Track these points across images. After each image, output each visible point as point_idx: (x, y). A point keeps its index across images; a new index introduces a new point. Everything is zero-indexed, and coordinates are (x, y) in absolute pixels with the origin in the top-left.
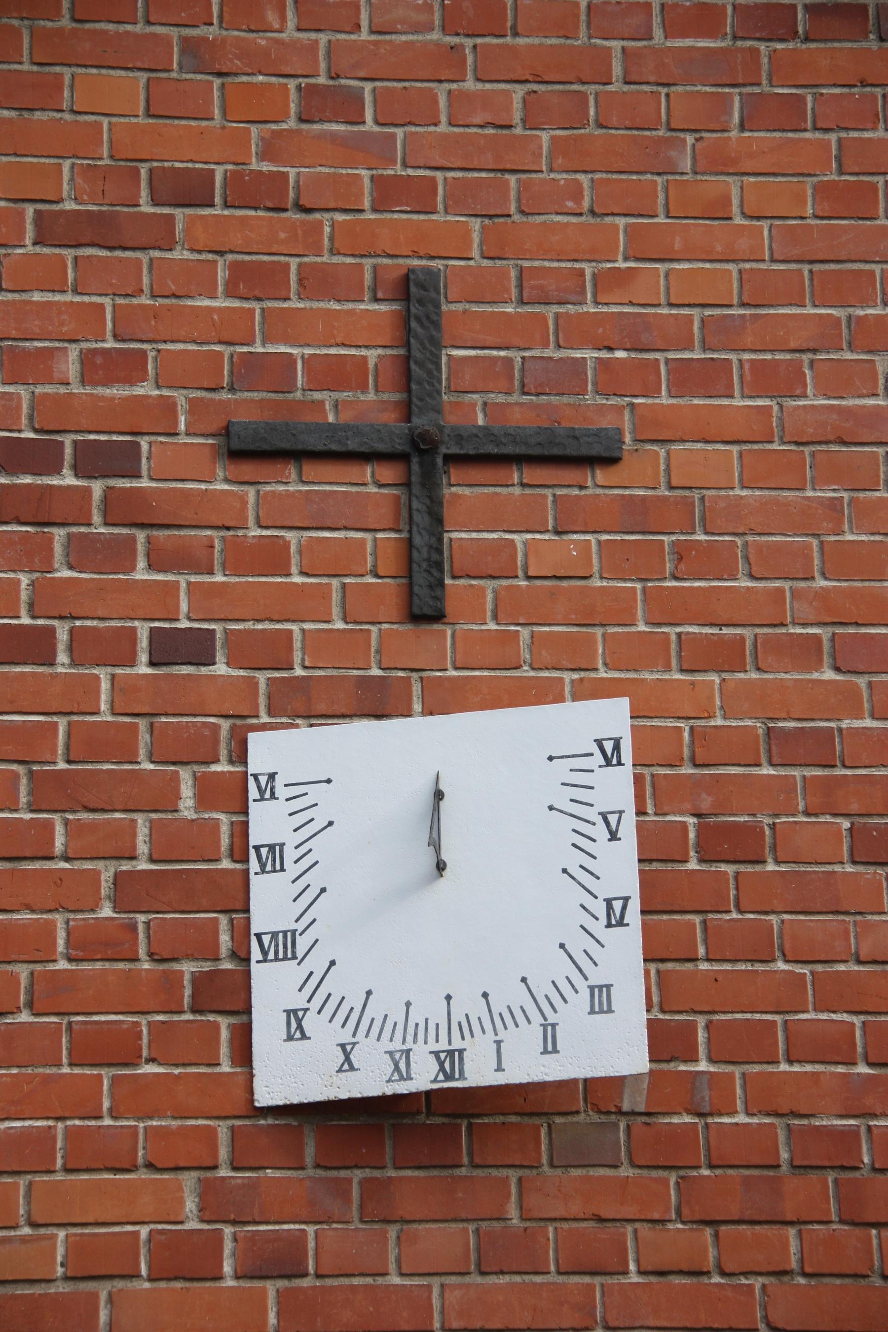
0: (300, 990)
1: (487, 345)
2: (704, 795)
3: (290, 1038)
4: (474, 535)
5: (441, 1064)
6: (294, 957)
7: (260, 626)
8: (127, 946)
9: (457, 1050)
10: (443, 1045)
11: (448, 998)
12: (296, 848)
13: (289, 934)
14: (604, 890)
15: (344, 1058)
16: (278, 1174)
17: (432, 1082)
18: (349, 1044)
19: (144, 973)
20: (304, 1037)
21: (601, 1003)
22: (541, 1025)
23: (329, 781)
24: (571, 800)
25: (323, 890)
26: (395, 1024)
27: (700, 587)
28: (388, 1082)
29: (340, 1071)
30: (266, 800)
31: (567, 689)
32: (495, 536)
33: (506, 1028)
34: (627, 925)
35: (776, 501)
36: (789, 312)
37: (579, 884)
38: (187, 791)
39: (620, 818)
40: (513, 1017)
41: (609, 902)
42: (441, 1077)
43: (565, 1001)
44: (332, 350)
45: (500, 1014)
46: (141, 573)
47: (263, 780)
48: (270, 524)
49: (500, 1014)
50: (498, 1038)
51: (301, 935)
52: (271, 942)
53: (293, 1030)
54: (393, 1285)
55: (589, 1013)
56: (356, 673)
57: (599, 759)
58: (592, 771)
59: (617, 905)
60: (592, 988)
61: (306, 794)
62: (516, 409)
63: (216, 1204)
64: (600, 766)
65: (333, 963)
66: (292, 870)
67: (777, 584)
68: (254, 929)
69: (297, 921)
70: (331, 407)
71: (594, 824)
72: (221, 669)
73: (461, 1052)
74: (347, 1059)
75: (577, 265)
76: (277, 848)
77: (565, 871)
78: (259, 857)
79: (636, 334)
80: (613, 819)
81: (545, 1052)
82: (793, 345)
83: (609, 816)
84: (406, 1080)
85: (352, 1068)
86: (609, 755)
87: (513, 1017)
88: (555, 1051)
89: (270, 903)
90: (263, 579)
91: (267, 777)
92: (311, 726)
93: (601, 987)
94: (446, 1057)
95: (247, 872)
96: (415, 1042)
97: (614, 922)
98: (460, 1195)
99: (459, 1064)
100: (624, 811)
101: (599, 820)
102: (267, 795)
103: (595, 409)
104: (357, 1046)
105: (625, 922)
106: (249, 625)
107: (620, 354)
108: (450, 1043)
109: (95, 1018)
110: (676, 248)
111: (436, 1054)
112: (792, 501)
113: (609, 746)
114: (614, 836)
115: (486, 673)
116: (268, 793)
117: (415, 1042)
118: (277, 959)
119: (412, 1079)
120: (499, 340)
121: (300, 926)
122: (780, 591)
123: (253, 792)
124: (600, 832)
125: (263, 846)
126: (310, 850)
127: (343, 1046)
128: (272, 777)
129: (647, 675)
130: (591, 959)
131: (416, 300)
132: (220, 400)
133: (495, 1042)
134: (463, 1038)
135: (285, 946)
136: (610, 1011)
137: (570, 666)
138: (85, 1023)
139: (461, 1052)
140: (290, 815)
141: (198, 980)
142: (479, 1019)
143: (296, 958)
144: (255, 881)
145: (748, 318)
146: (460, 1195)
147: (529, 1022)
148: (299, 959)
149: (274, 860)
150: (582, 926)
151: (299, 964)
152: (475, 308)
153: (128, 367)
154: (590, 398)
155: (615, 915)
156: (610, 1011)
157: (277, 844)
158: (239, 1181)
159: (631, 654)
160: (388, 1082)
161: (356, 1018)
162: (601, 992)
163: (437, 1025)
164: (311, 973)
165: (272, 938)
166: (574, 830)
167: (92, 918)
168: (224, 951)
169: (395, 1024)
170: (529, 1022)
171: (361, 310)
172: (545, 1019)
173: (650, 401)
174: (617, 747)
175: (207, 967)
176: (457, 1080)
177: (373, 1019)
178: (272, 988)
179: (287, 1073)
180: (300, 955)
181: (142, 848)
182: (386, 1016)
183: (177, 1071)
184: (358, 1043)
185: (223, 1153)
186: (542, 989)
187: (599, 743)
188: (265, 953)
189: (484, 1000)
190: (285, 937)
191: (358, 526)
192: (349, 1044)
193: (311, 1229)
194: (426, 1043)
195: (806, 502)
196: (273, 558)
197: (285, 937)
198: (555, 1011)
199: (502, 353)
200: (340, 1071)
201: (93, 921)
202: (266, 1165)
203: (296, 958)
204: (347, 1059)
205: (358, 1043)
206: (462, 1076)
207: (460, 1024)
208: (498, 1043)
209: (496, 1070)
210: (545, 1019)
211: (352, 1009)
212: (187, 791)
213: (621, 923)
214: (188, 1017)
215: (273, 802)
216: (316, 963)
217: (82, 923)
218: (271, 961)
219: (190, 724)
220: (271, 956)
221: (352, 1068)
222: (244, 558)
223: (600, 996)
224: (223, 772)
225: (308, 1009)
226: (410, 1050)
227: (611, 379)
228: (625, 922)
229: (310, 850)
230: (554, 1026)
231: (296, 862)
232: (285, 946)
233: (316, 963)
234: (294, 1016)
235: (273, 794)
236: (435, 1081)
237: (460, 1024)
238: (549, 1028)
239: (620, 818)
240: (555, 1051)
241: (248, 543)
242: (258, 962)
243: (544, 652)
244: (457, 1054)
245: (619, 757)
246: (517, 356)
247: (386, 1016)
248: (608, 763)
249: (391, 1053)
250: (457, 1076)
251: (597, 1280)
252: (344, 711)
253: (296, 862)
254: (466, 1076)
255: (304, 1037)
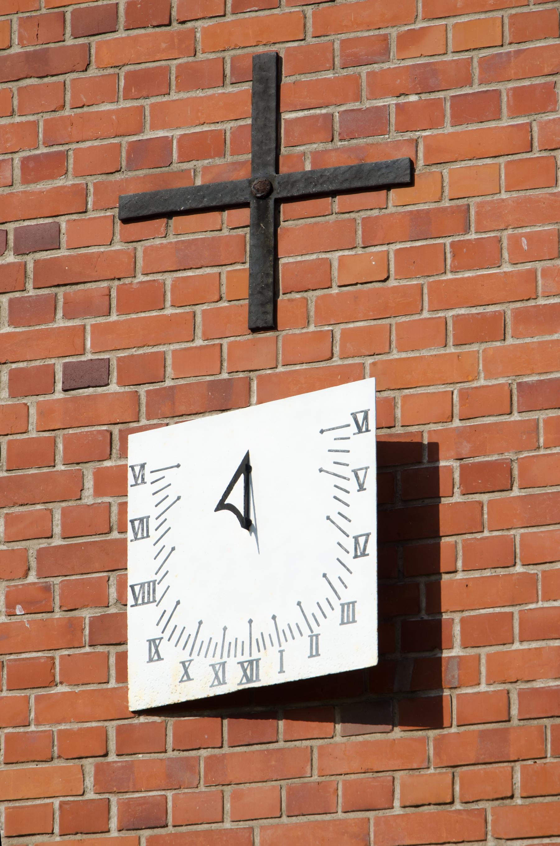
0: (157, 625)
1: (312, 106)
2: (465, 443)
3: (151, 660)
4: (299, 259)
5: (245, 671)
6: (154, 601)
7: (141, 351)
8: (44, 602)
9: (255, 660)
10: (246, 657)
11: (251, 621)
12: (157, 519)
13: (151, 584)
14: (353, 529)
15: (184, 672)
16: (147, 757)
17: (238, 684)
18: (187, 661)
19: (55, 621)
20: (160, 659)
21: (348, 616)
22: (309, 636)
23: (178, 466)
24: (335, 463)
25: (173, 549)
26: (217, 643)
27: (469, 277)
28: (211, 687)
29: (181, 681)
30: (139, 484)
31: (368, 370)
32: (314, 257)
33: (286, 641)
34: (368, 555)
35: (529, 200)
36: (544, 44)
37: (338, 526)
38: (89, 483)
39: (366, 472)
40: (292, 632)
41: (356, 538)
42: (244, 680)
43: (325, 617)
44: (202, 129)
45: (283, 631)
46: (60, 322)
47: (137, 469)
48: (149, 272)
49: (283, 631)
50: (281, 649)
51: (158, 584)
52: (140, 591)
53: (153, 654)
54: (224, 829)
55: (340, 624)
56: (208, 378)
57: (354, 428)
58: (349, 438)
59: (362, 540)
60: (343, 605)
61: (164, 477)
62: (333, 154)
63: (107, 781)
64: (354, 434)
65: (178, 603)
66: (154, 535)
67: (528, 266)
68: (130, 583)
69: (156, 574)
70: (200, 173)
71: (349, 480)
72: (114, 387)
73: (258, 660)
74: (186, 673)
75: (382, 32)
76: (145, 520)
77: (328, 518)
78: (133, 528)
79: (425, 80)
80: (361, 474)
81: (311, 656)
82: (546, 71)
83: (359, 472)
84: (222, 684)
85: (189, 679)
86: (361, 424)
87: (292, 632)
88: (318, 654)
89: (140, 561)
90: (143, 315)
91: (139, 467)
92: (177, 423)
93: (348, 604)
94: (248, 665)
95: (126, 540)
96: (229, 656)
97: (359, 554)
98: (273, 763)
99: (256, 670)
100: (369, 467)
101: (352, 476)
102: (140, 481)
103: (388, 146)
104: (192, 662)
105: (366, 553)
106: (133, 351)
107: (413, 98)
108: (251, 655)
109: (24, 656)
110: (458, 6)
111: (241, 663)
112: (542, 198)
113: (360, 417)
114: (361, 488)
115: (305, 366)
116: (140, 480)
117: (229, 656)
118: (143, 603)
119: (226, 683)
120: (321, 101)
121: (158, 577)
122: (534, 272)
123: (131, 480)
124: (353, 485)
125: (136, 520)
126: (166, 520)
127: (183, 663)
128: (143, 466)
129: (425, 353)
130: (343, 583)
131: (268, 78)
132: (115, 181)
133: (279, 651)
134: (259, 651)
135: (149, 594)
136: (354, 621)
137: (368, 353)
138: (15, 660)
139: (258, 660)
140: (154, 494)
141: (94, 621)
142: (270, 635)
143: (155, 601)
144: (130, 545)
145: (512, 54)
146: (273, 763)
147: (301, 635)
148: (158, 601)
149: (143, 530)
150: (338, 559)
151: (157, 605)
152: (303, 78)
153: (54, 165)
154: (394, 136)
155: (360, 548)
156: (354, 621)
157: (145, 518)
158: (119, 764)
159: (371, 344)
160: (211, 687)
161: (191, 643)
162: (348, 607)
163: (243, 642)
164: (165, 611)
165: (141, 587)
166: (336, 486)
167: (21, 585)
168: (112, 601)
169: (217, 643)
170: (301, 635)
171: (219, 94)
172: (312, 632)
173: (435, 132)
174: (366, 418)
175: (98, 612)
176: (255, 681)
177: (203, 642)
178: (140, 624)
179: (150, 684)
180: (158, 599)
181: (57, 530)
182: (211, 639)
183: (77, 689)
184: (192, 660)
185: (112, 746)
186: (310, 609)
187: (354, 415)
188: (136, 599)
189: (273, 621)
190: (149, 586)
191: (213, 264)
192: (187, 661)
193: (170, 795)
194: (235, 656)
195: (553, 198)
196: (152, 297)
197: (149, 586)
198: (318, 625)
199: (324, 111)
200: (181, 681)
201: (21, 587)
202: (138, 752)
203: (155, 601)
204: (186, 673)
205: (192, 660)
206: (258, 679)
207: (257, 640)
208: (281, 652)
209: (279, 673)
210: (312, 632)
211: (190, 635)
212: (89, 483)
213: (364, 554)
214: (88, 649)
215: (143, 486)
216: (168, 604)
217: (14, 588)
218: (140, 604)
219: (89, 433)
220: (140, 601)
221: (189, 679)
222: (134, 300)
223: (348, 611)
224: (111, 467)
225: (162, 638)
226: (225, 662)
227: (408, 118)
228: (366, 553)
229: (166, 520)
230: (317, 636)
231: (156, 530)
232: (149, 594)
233: (168, 604)
234: (153, 643)
235: (143, 479)
236: (241, 683)
237: (257, 640)
238: (314, 638)
239: (366, 472)
240: (318, 654)
241: (132, 288)
242: (132, 606)
243: (348, 345)
244: (255, 662)
245: (367, 425)
246: (336, 111)
247: (211, 639)
248: (360, 431)
249: (213, 666)
250: (254, 679)
251: (371, 815)
252: (199, 410)
253: (156, 530)
254: (260, 678)
255: (160, 659)
